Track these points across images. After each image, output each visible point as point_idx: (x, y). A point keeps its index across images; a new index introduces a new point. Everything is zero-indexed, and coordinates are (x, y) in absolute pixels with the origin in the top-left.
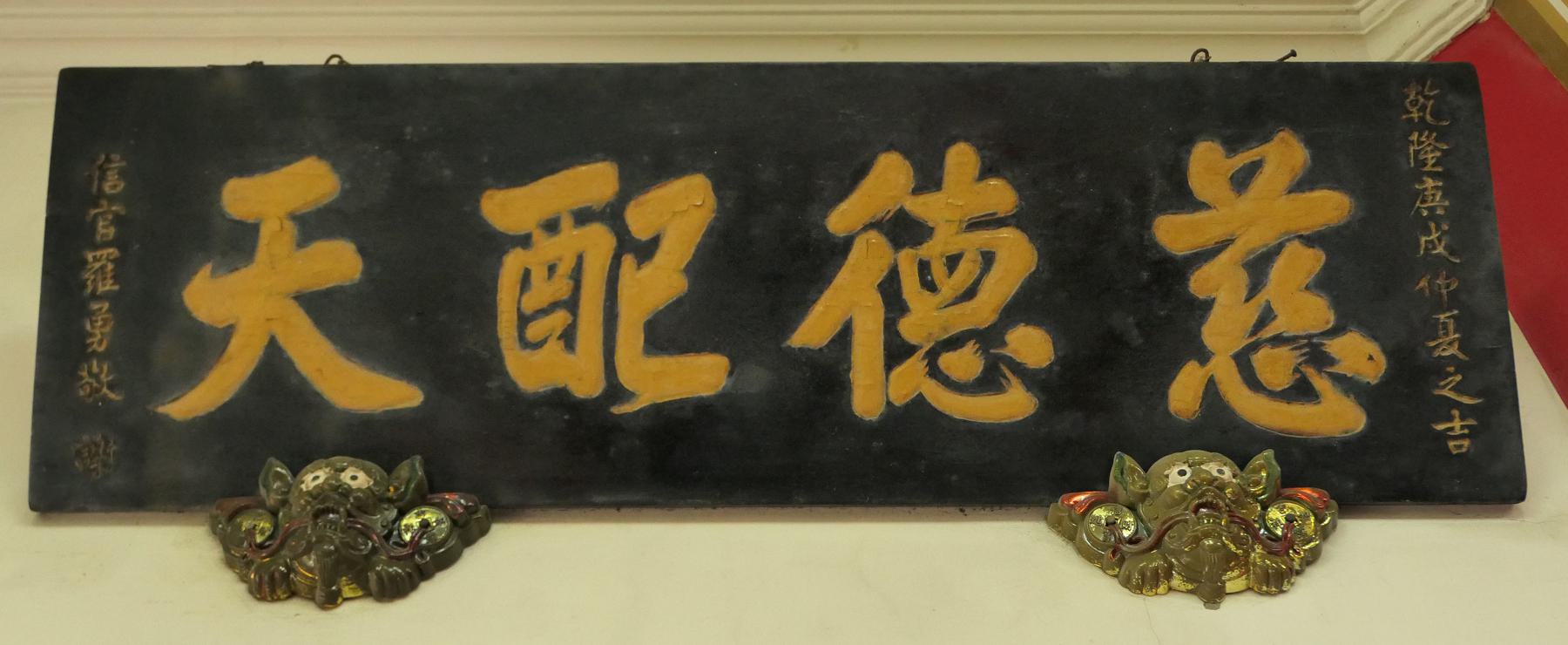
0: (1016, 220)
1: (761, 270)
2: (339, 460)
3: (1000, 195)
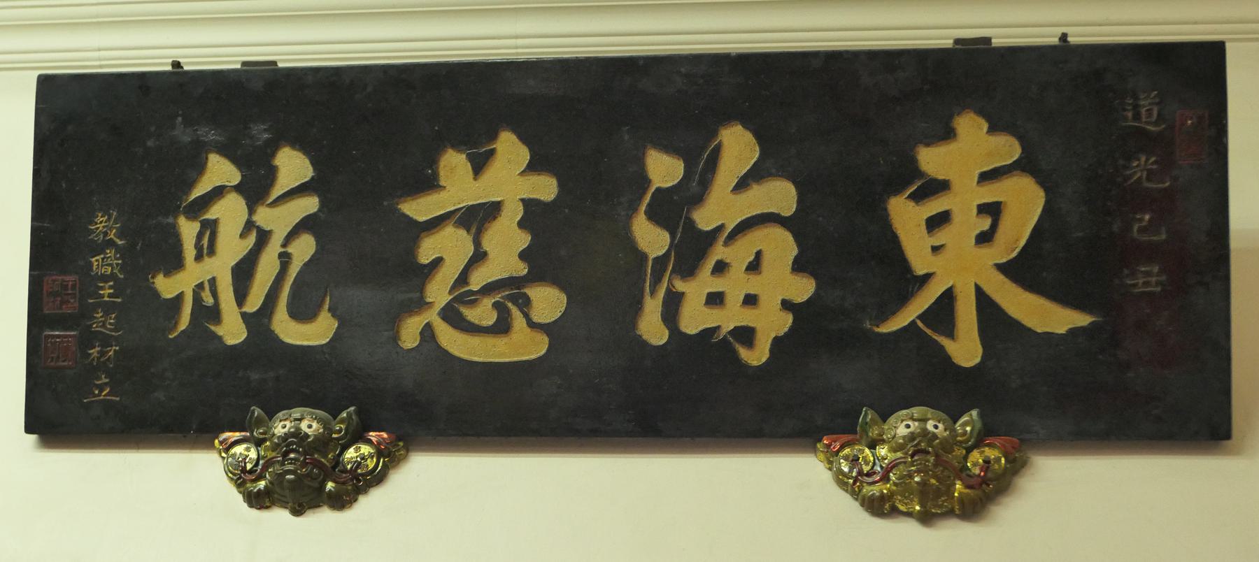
0: (1024, 165)
1: (366, 247)
2: (297, 412)
3: (1007, 149)
